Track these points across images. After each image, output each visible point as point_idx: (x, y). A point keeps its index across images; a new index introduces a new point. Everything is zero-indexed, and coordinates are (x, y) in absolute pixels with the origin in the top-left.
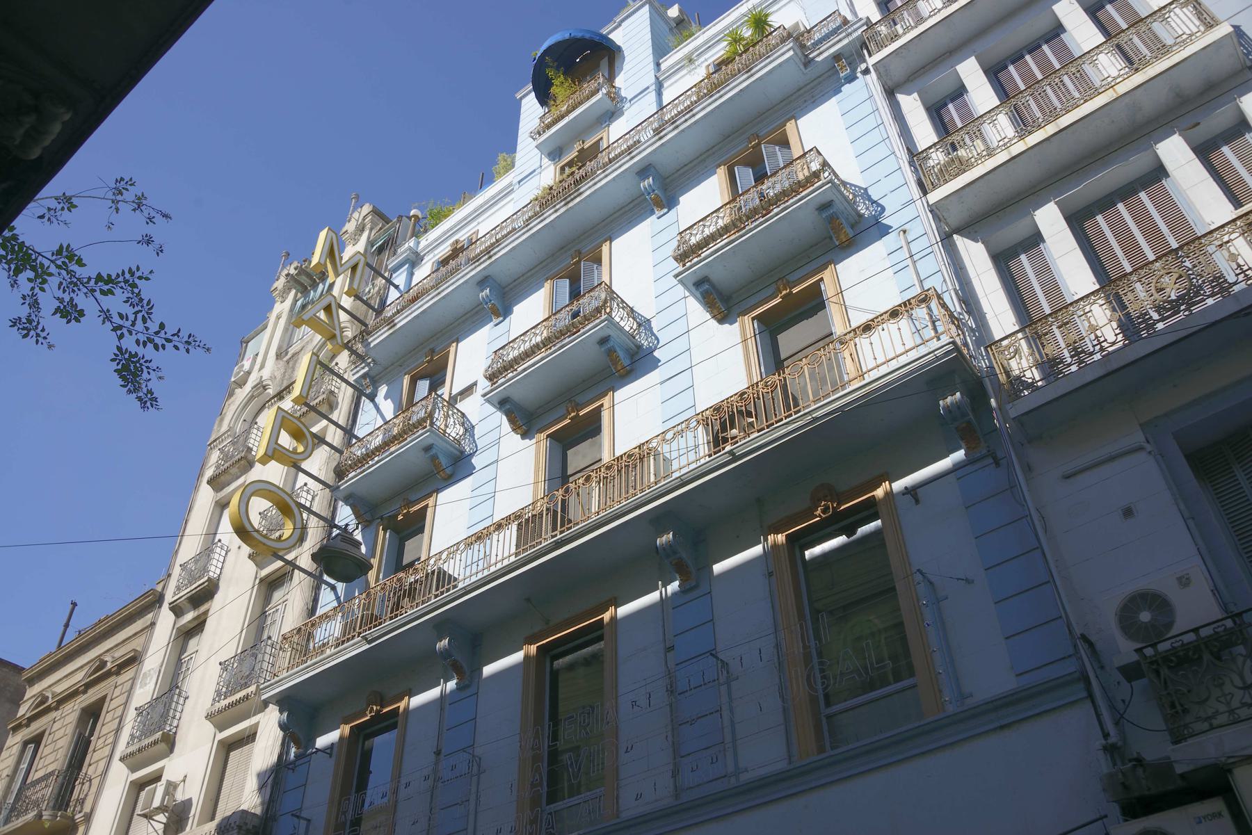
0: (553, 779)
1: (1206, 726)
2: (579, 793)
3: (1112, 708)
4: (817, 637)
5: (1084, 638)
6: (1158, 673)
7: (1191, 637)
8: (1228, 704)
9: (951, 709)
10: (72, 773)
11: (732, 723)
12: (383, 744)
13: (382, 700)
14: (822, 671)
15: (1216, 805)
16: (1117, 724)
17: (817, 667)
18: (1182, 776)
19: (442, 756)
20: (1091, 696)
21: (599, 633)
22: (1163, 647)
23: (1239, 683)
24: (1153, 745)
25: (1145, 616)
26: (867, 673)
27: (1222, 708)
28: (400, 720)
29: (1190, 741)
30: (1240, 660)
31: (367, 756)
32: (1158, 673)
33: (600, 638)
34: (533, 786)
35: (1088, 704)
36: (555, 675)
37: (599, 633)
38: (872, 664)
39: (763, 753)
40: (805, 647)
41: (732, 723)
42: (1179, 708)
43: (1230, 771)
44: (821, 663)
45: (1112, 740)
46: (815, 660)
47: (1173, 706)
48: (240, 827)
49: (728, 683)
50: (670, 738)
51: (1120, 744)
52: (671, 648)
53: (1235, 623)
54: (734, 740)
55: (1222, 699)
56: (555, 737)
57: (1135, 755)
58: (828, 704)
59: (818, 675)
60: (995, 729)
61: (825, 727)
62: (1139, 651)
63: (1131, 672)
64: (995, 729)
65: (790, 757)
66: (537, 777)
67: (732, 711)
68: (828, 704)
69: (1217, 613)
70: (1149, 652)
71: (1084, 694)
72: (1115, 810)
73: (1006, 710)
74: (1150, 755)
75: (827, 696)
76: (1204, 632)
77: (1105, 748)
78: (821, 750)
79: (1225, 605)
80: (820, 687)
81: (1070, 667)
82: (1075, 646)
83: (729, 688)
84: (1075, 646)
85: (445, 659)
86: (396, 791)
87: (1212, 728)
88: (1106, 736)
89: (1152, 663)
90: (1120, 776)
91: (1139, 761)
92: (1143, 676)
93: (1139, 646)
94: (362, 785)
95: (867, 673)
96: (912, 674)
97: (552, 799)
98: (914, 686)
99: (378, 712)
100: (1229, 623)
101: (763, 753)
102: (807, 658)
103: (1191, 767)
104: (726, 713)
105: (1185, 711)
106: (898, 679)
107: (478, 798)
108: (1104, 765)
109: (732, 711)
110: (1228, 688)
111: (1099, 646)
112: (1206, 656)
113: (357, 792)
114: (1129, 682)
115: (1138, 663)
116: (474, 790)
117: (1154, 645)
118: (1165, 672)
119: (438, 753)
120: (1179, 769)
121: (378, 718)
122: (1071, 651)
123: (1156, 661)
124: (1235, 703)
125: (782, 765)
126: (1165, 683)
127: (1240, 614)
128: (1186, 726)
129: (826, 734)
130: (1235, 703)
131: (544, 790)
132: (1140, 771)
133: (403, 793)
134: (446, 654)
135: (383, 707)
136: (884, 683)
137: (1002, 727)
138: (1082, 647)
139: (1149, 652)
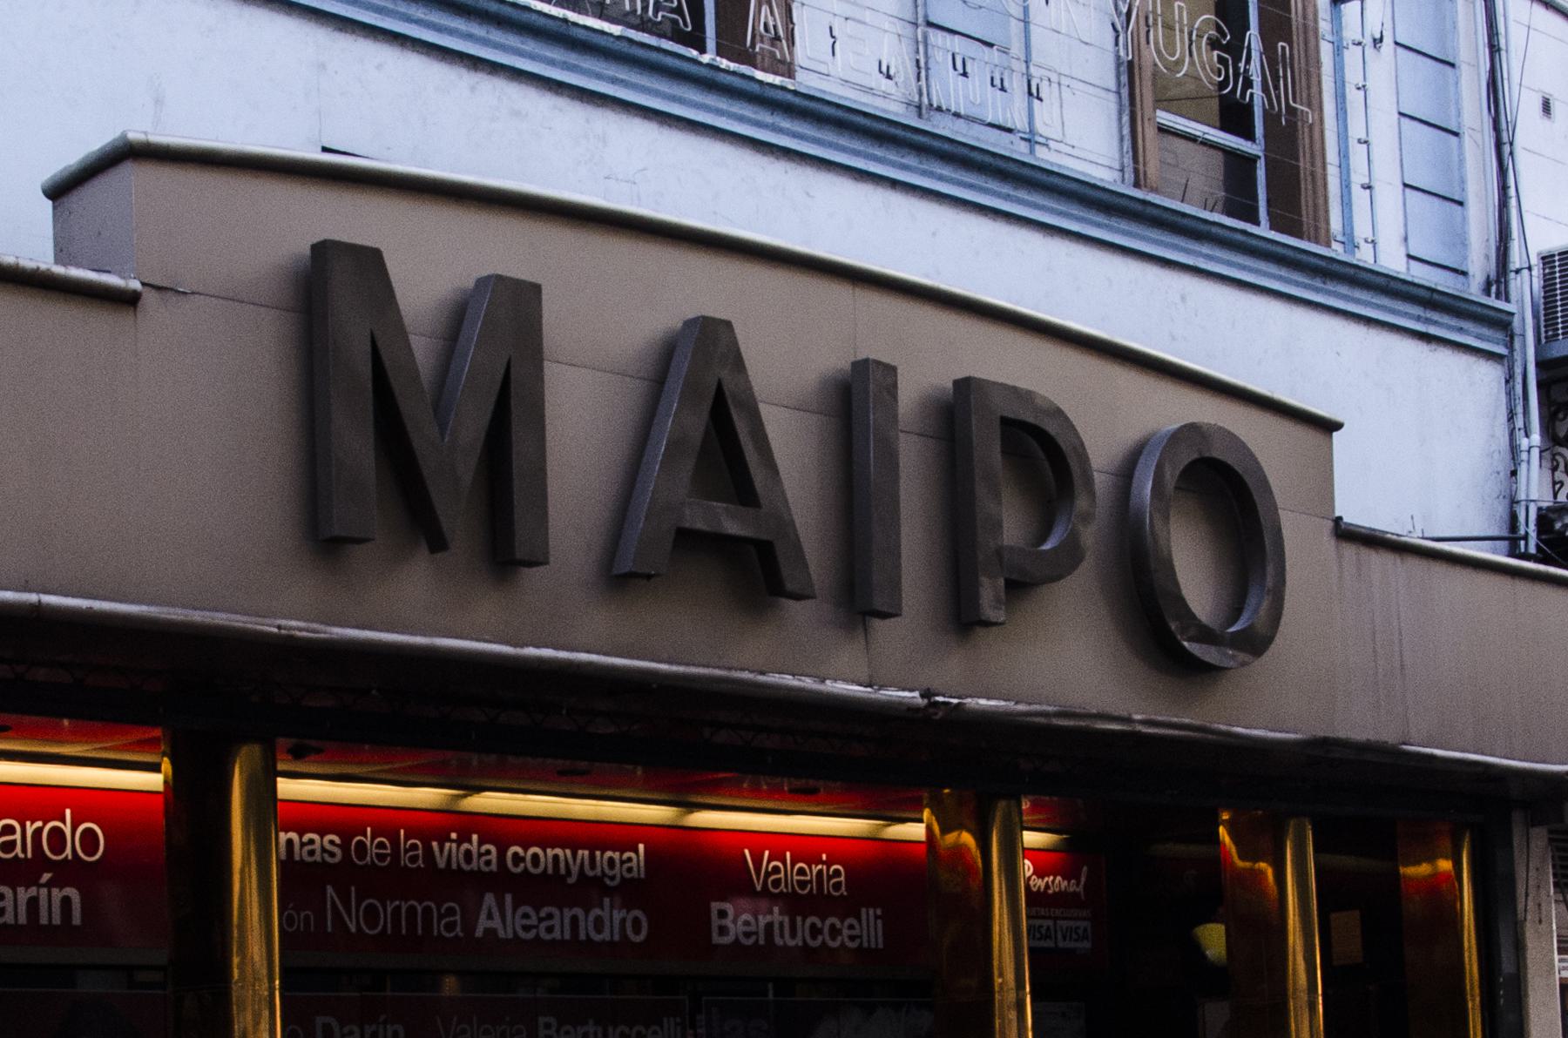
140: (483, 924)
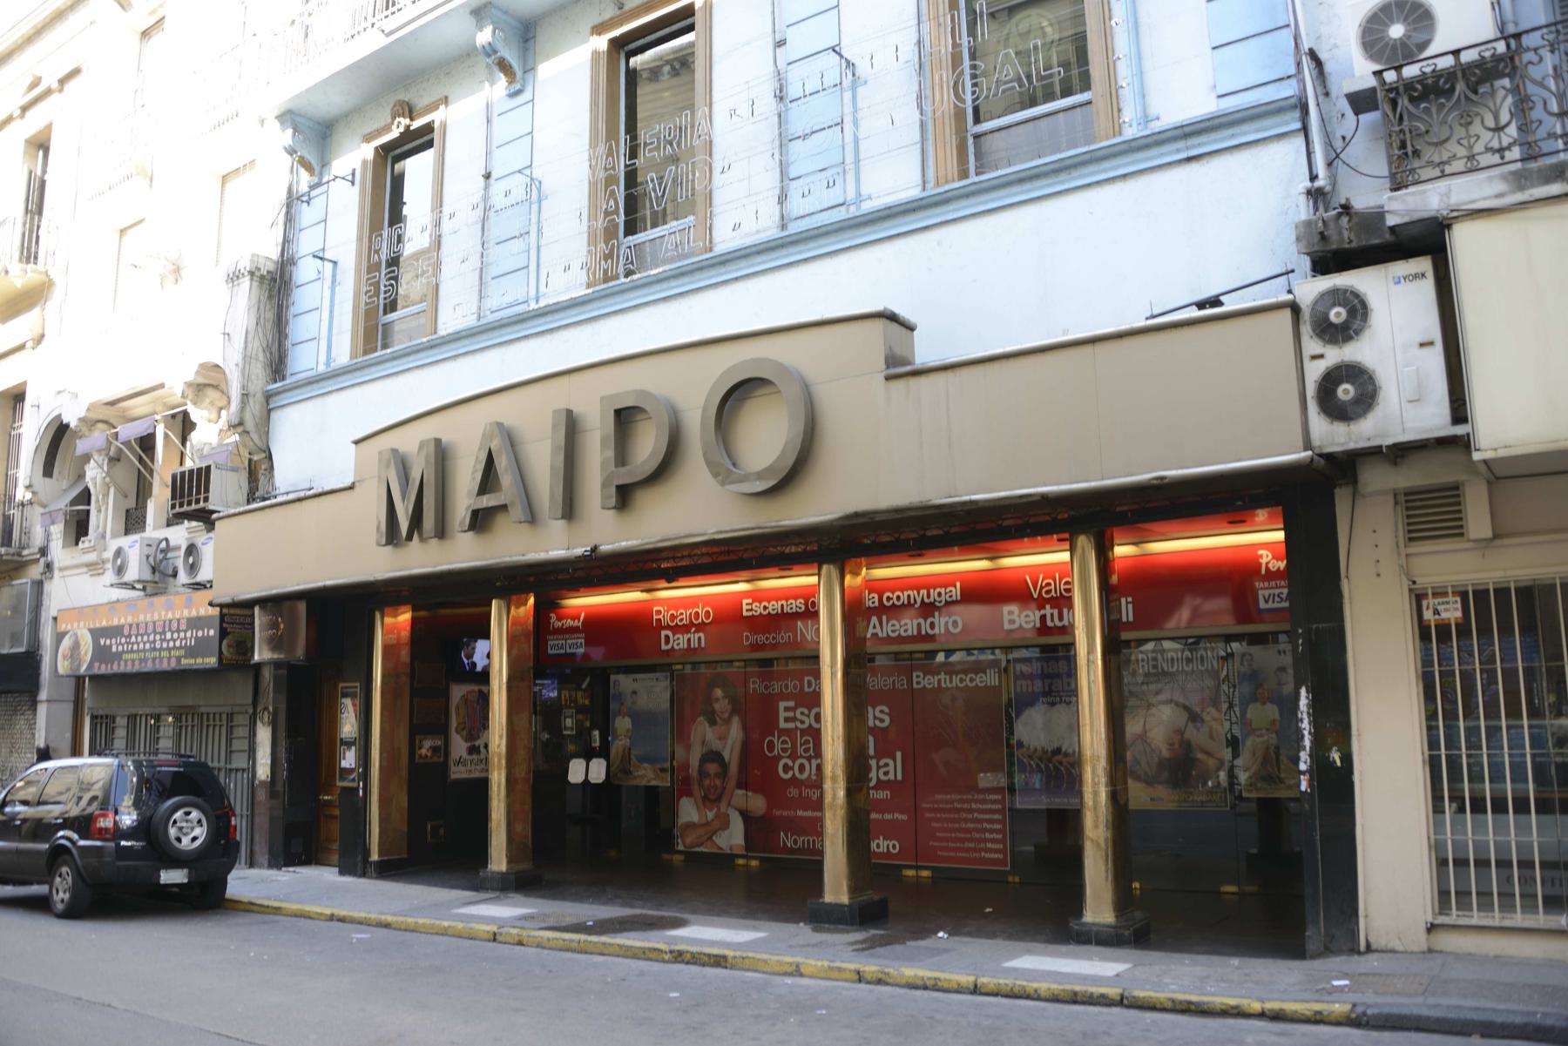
0: (632, 205)
1: (1437, 172)
2: (665, 223)
3: (1328, 143)
4: (972, 31)
5: (1313, 54)
6: (1394, 103)
7: (1448, 62)
8: (1471, 147)
9: (1130, 133)
10: (32, 220)
11: (856, 140)
12: (417, 169)
13: (411, 112)
14: (974, 76)
15: (1424, 264)
16: (1329, 164)
17: (967, 71)
18: (1393, 229)
19: (492, 180)
20: (1305, 130)
21: (689, 21)
22: (1410, 71)
23: (1491, 123)
24: (1368, 190)
25: (1396, 31)
26: (1030, 82)
27: (1462, 152)
28: (436, 136)
29: (1411, 189)
30: (1501, 93)
31: (398, 182)
32: (1394, 103)
33: (691, 28)
34: (607, 213)
35: (1299, 141)
36: (632, 76)
37: (689, 21)
38: (1038, 73)
39: (894, 175)
40: (955, 45)
41: (856, 140)
42: (1409, 149)
43: (1449, 227)
44: (974, 67)
45: (1320, 183)
46: (967, 63)
47: (1403, 145)
48: (252, 273)
49: (854, 88)
50: (777, 156)
51: (1328, 188)
52: (780, 44)
53: (1508, 46)
54: (857, 161)
55: (1465, 142)
56: (633, 153)
57: (1343, 202)
58: (977, 120)
59: (968, 84)
60: (1180, 162)
61: (971, 149)
62: (1378, 74)
63: (1361, 102)
64: (1180, 162)
65: (924, 182)
66: (612, 203)
67: (856, 123)
68: (977, 120)
69: (1487, 30)
70: (1390, 76)
71: (1298, 125)
72: (1306, 263)
73: (1195, 139)
74: (1361, 203)
75: (976, 110)
76: (1466, 57)
77: (1309, 193)
78: (964, 174)
79: (1503, 23)
80: (969, 98)
81: (1288, 90)
82: (1299, 64)
83: (854, 97)
84: (1299, 64)
85: (489, 56)
86: (438, 224)
87: (1443, 175)
88: (1313, 178)
89: (1390, 90)
90: (1320, 224)
91: (1346, 208)
92: (1376, 108)
93: (1378, 67)
94: (396, 217)
95: (1030, 82)
96: (1086, 85)
97: (631, 229)
98: (1089, 103)
99: (408, 127)
100: (1501, 47)
101: (894, 175)
102: (956, 60)
103: (1406, 219)
104: (848, 126)
105: (1417, 153)
106: (1067, 92)
107: (539, 231)
108: (1302, 210)
109: (856, 123)
110: (1476, 128)
111: (1328, 68)
112: (1460, 87)
113: (391, 225)
114: (1357, 114)
115: (1373, 90)
116: (534, 220)
117: (1398, 69)
118: (1404, 102)
119: (487, 176)
120: (1391, 221)
121: (408, 135)
122: (1293, 71)
123: (1397, 89)
124: (1479, 147)
125: (915, 192)
126: (1401, 118)
127: (1517, 36)
128: (1413, 171)
129: (972, 158)
130: (1479, 147)
131: (621, 219)
132: (1345, 219)
133: (447, 226)
134: (490, 50)
135: (412, 119)
136: (1049, 97)
137: (1189, 159)
138: (1306, 61)
139: (1390, 76)
140: (871, 631)
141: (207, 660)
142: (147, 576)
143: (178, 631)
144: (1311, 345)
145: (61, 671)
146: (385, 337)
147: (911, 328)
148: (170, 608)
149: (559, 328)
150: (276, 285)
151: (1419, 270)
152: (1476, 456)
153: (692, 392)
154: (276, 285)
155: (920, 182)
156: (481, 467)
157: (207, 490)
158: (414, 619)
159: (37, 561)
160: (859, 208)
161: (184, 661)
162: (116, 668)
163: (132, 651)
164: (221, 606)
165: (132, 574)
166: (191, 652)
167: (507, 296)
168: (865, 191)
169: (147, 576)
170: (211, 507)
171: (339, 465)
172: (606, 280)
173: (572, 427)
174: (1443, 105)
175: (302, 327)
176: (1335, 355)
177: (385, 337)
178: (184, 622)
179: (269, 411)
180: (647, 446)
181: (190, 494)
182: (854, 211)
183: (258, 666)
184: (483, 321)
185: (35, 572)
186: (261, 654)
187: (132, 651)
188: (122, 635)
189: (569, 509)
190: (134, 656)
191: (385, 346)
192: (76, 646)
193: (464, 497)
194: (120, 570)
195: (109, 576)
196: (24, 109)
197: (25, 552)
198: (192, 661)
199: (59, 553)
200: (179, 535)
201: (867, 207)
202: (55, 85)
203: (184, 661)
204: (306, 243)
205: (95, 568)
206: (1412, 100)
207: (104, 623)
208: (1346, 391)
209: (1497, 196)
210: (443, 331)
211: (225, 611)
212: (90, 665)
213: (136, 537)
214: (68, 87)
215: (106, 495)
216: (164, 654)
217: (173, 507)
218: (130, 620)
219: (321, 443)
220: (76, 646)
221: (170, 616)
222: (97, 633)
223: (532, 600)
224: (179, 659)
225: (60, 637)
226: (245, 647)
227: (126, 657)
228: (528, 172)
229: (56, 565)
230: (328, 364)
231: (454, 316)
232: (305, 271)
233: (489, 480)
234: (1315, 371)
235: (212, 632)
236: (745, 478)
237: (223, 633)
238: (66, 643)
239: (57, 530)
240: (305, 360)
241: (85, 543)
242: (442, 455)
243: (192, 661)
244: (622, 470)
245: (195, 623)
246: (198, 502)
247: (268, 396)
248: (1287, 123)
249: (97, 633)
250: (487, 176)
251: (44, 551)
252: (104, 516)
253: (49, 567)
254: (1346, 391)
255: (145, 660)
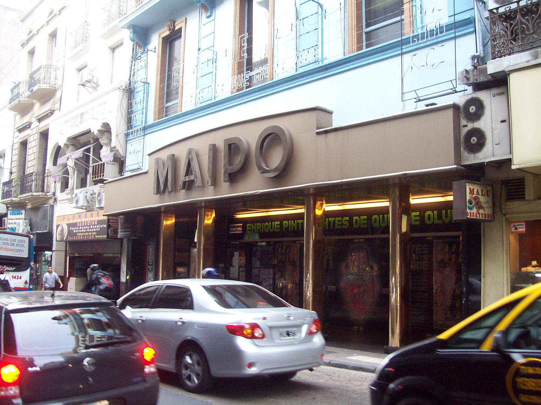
39: (335, 49)
43: (509, 74)
78: (360, 48)
119: (199, 50)
125: (341, 57)
141: (104, 236)
142: (86, 204)
143: (95, 225)
144: (463, 122)
145: (58, 240)
146: (166, 112)
147: (331, 113)
148: (92, 216)
149: (183, 122)
150: (130, 92)
151: (502, 91)
152: (513, 167)
153: (251, 138)
154: (130, 92)
155: (343, 53)
156: (186, 165)
157: (103, 172)
158: (175, 222)
159: (51, 198)
160: (323, 62)
161: (96, 237)
162: (75, 238)
163: (80, 232)
164: (108, 215)
165: (81, 204)
166: (98, 233)
167: (207, 97)
168: (325, 57)
169: (86, 204)
170: (105, 179)
171: (147, 165)
172: (238, 91)
173: (214, 149)
174: (533, 18)
175: (138, 107)
176: (470, 126)
177: (166, 112)
178: (96, 221)
179: (127, 141)
180: (238, 160)
181: (98, 174)
182: (321, 64)
183: (122, 240)
184: (197, 107)
185: (51, 202)
186: (120, 235)
187: (80, 232)
188: (77, 226)
189: (215, 182)
190: (81, 234)
191: (166, 116)
192: (62, 230)
193: (182, 177)
194: (77, 202)
195: (74, 205)
196: (48, 22)
197: (48, 194)
198: (99, 237)
199: (60, 196)
200: (97, 188)
201: (326, 62)
202: (58, 13)
203: (96, 237)
204: (140, 76)
205: (70, 200)
206: (523, 16)
207: (71, 222)
208: (474, 140)
209: (528, 61)
210: (184, 110)
211: (110, 218)
212: (67, 238)
213: (82, 189)
214: (63, 12)
215: (74, 173)
216: (90, 234)
217: (93, 178)
218: (79, 221)
219: (141, 155)
220: (62, 230)
221: (92, 219)
222: (69, 225)
223: (214, 215)
224: (95, 235)
225: (58, 226)
226: (116, 232)
227: (78, 234)
228: (212, 48)
229: (58, 199)
230: (146, 123)
231: (188, 105)
232: (139, 87)
233: (189, 170)
234: (464, 131)
235: (105, 226)
236: (269, 171)
237: (109, 226)
238: (60, 228)
239: (59, 185)
240: (138, 120)
241: (67, 191)
242: (174, 159)
243: (99, 237)
244: (231, 167)
245: (100, 222)
246: (100, 176)
247: (127, 135)
248: (469, 28)
249: (69, 225)
250: (199, 50)
251: (54, 194)
252: (73, 181)
253: (55, 200)
254: (474, 140)
255: (84, 236)
